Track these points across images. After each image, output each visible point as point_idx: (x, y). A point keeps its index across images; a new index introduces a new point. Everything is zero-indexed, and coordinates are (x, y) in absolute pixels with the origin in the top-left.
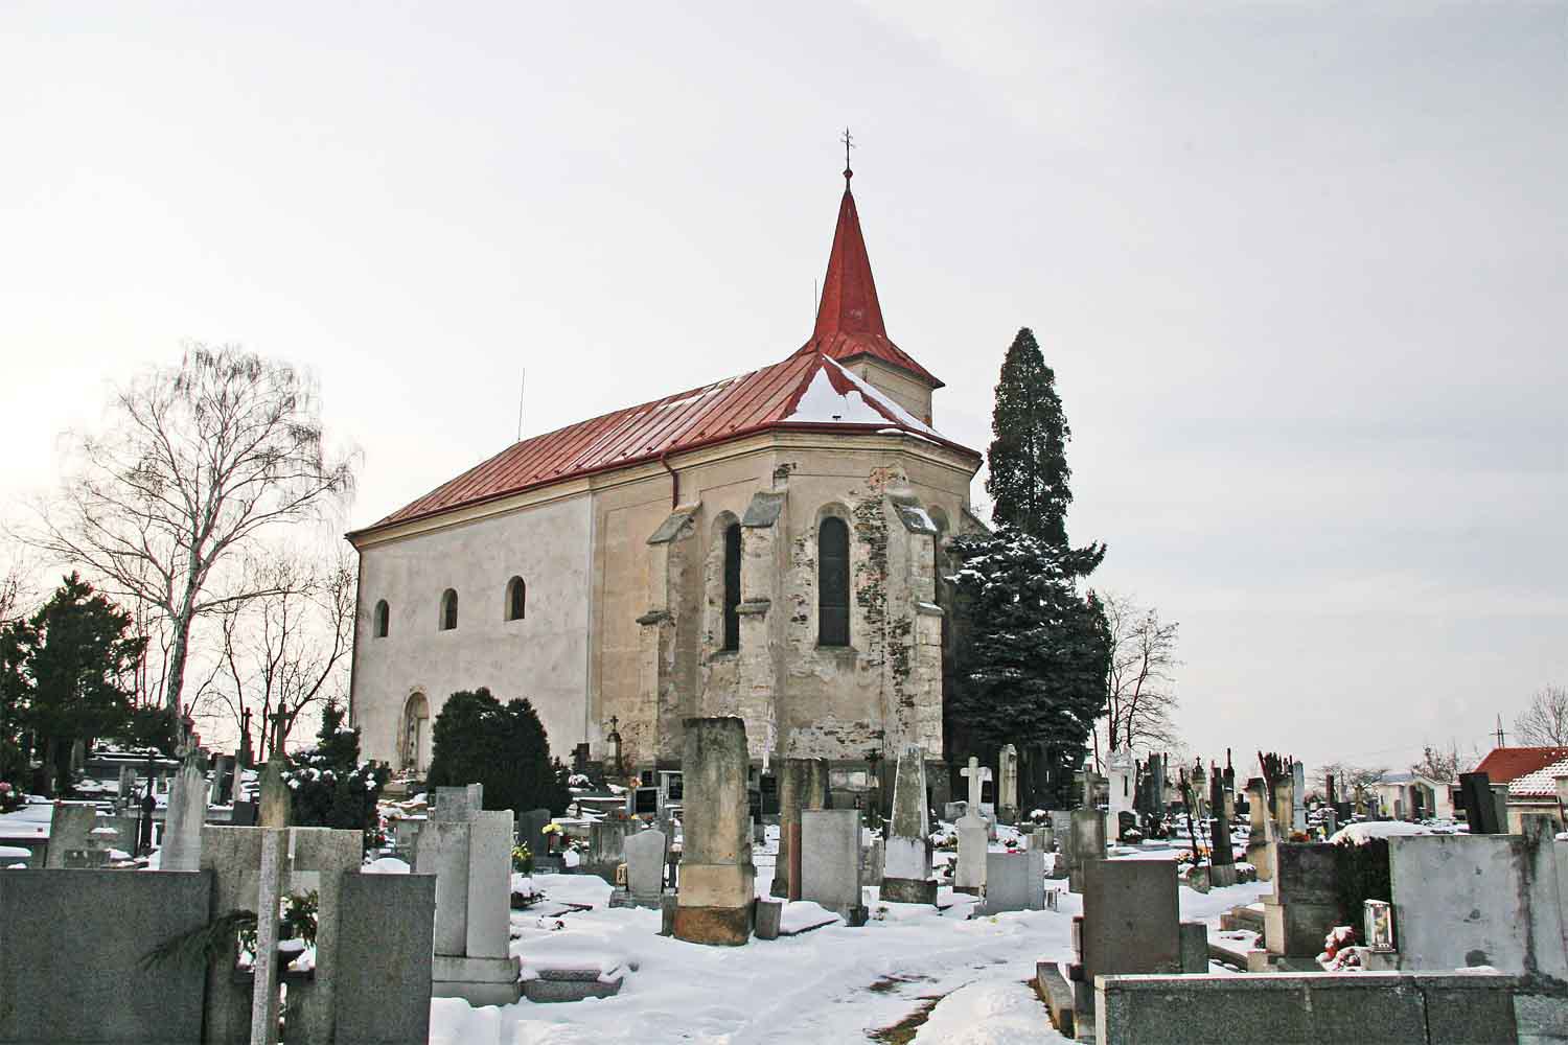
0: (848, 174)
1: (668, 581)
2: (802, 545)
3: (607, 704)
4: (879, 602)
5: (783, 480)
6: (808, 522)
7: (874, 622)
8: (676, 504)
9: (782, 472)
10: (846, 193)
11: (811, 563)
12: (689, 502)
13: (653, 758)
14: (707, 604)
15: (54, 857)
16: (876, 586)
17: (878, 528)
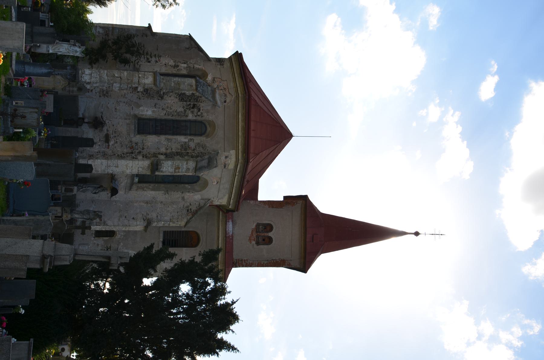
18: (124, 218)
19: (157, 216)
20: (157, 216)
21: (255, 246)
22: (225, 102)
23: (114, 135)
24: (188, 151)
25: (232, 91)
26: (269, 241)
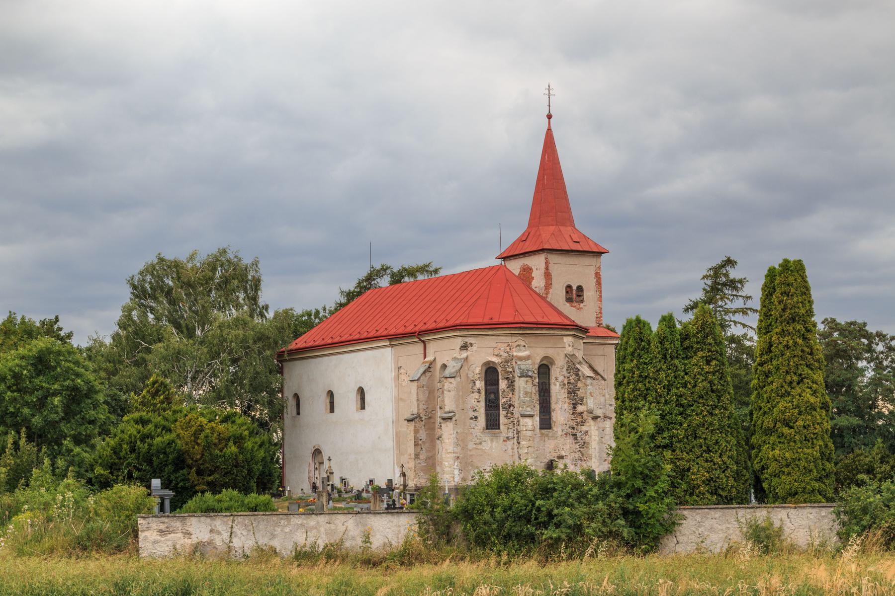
0: (549, 117)
1: (418, 400)
2: (475, 382)
3: (402, 457)
4: (512, 408)
5: (465, 351)
6: (477, 369)
7: (510, 418)
8: (425, 357)
9: (464, 347)
10: (548, 130)
11: (479, 391)
12: (429, 358)
13: (413, 485)
14: (439, 408)
15: (534, 391)
16: (510, 401)
17: (511, 372)
18: (603, 439)
19: (601, 408)
20: (601, 408)
21: (584, 304)
22: (525, 346)
23: (557, 451)
24: (566, 383)
25: (514, 339)
26: (580, 289)
